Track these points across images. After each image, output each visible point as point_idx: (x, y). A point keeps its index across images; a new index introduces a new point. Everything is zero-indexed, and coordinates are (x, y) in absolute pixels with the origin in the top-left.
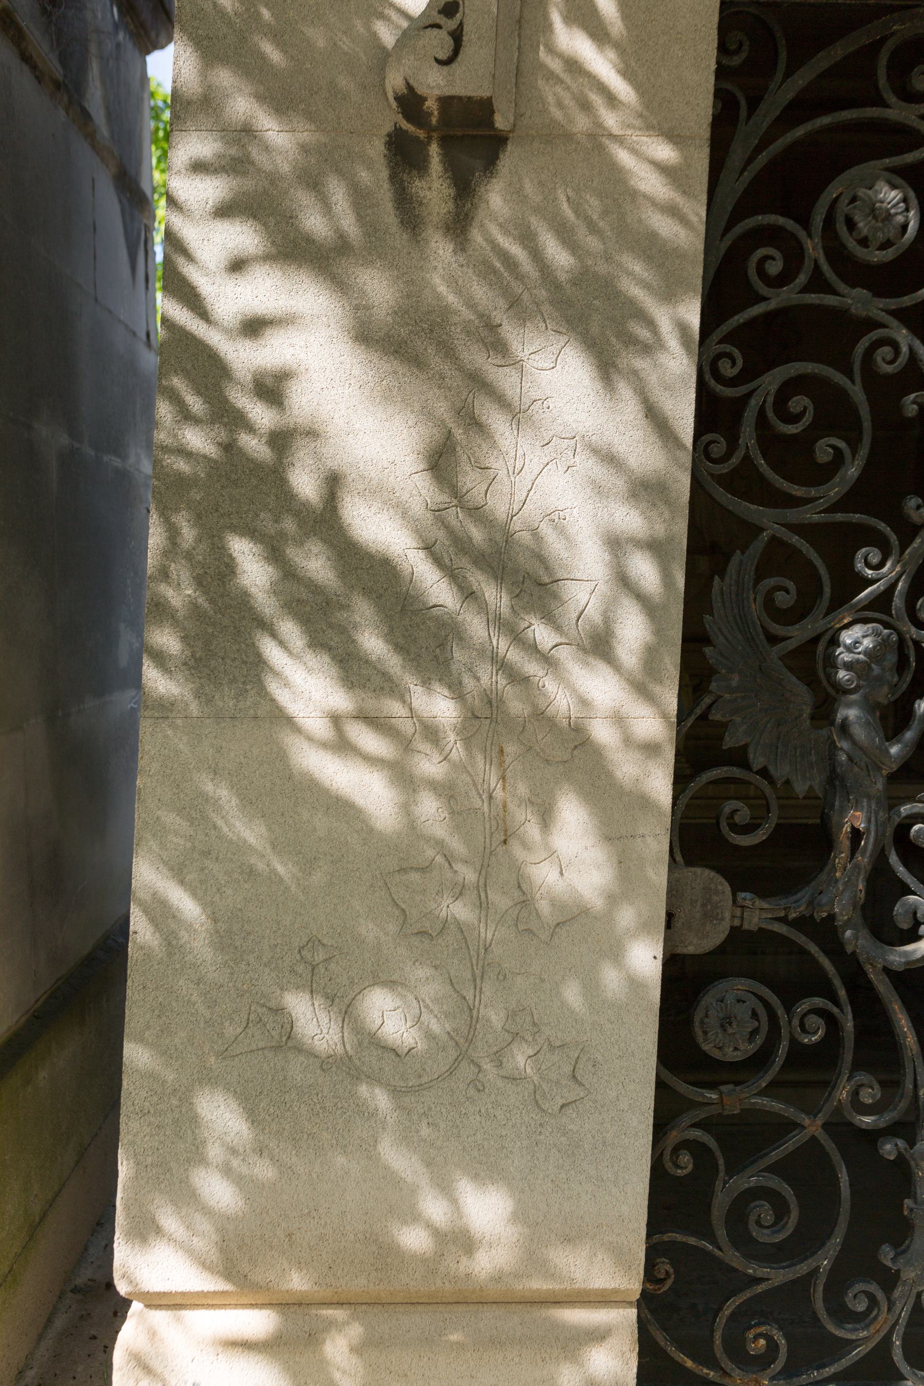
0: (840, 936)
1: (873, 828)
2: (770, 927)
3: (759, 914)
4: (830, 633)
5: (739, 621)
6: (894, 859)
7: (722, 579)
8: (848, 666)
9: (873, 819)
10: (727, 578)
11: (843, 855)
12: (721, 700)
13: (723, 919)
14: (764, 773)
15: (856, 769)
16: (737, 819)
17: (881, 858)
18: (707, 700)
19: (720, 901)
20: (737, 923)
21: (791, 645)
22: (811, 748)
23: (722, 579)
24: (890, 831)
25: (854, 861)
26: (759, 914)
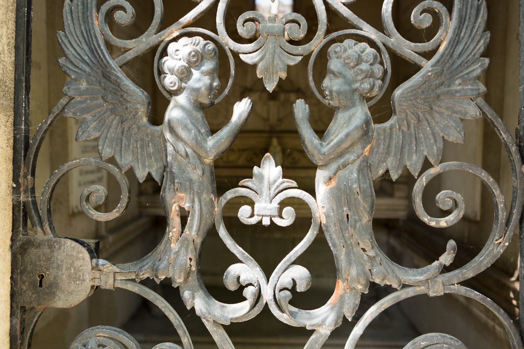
0: (181, 295)
1: (197, 207)
2: (124, 287)
4: (162, 45)
6: (223, 232)
9: (196, 200)
11: (175, 230)
12: (72, 101)
13: (84, 280)
14: (112, 160)
15: (179, 158)
17: (212, 233)
18: (63, 101)
20: (96, 283)
21: (129, 56)
22: (149, 141)
25: (184, 234)
26: (113, 276)
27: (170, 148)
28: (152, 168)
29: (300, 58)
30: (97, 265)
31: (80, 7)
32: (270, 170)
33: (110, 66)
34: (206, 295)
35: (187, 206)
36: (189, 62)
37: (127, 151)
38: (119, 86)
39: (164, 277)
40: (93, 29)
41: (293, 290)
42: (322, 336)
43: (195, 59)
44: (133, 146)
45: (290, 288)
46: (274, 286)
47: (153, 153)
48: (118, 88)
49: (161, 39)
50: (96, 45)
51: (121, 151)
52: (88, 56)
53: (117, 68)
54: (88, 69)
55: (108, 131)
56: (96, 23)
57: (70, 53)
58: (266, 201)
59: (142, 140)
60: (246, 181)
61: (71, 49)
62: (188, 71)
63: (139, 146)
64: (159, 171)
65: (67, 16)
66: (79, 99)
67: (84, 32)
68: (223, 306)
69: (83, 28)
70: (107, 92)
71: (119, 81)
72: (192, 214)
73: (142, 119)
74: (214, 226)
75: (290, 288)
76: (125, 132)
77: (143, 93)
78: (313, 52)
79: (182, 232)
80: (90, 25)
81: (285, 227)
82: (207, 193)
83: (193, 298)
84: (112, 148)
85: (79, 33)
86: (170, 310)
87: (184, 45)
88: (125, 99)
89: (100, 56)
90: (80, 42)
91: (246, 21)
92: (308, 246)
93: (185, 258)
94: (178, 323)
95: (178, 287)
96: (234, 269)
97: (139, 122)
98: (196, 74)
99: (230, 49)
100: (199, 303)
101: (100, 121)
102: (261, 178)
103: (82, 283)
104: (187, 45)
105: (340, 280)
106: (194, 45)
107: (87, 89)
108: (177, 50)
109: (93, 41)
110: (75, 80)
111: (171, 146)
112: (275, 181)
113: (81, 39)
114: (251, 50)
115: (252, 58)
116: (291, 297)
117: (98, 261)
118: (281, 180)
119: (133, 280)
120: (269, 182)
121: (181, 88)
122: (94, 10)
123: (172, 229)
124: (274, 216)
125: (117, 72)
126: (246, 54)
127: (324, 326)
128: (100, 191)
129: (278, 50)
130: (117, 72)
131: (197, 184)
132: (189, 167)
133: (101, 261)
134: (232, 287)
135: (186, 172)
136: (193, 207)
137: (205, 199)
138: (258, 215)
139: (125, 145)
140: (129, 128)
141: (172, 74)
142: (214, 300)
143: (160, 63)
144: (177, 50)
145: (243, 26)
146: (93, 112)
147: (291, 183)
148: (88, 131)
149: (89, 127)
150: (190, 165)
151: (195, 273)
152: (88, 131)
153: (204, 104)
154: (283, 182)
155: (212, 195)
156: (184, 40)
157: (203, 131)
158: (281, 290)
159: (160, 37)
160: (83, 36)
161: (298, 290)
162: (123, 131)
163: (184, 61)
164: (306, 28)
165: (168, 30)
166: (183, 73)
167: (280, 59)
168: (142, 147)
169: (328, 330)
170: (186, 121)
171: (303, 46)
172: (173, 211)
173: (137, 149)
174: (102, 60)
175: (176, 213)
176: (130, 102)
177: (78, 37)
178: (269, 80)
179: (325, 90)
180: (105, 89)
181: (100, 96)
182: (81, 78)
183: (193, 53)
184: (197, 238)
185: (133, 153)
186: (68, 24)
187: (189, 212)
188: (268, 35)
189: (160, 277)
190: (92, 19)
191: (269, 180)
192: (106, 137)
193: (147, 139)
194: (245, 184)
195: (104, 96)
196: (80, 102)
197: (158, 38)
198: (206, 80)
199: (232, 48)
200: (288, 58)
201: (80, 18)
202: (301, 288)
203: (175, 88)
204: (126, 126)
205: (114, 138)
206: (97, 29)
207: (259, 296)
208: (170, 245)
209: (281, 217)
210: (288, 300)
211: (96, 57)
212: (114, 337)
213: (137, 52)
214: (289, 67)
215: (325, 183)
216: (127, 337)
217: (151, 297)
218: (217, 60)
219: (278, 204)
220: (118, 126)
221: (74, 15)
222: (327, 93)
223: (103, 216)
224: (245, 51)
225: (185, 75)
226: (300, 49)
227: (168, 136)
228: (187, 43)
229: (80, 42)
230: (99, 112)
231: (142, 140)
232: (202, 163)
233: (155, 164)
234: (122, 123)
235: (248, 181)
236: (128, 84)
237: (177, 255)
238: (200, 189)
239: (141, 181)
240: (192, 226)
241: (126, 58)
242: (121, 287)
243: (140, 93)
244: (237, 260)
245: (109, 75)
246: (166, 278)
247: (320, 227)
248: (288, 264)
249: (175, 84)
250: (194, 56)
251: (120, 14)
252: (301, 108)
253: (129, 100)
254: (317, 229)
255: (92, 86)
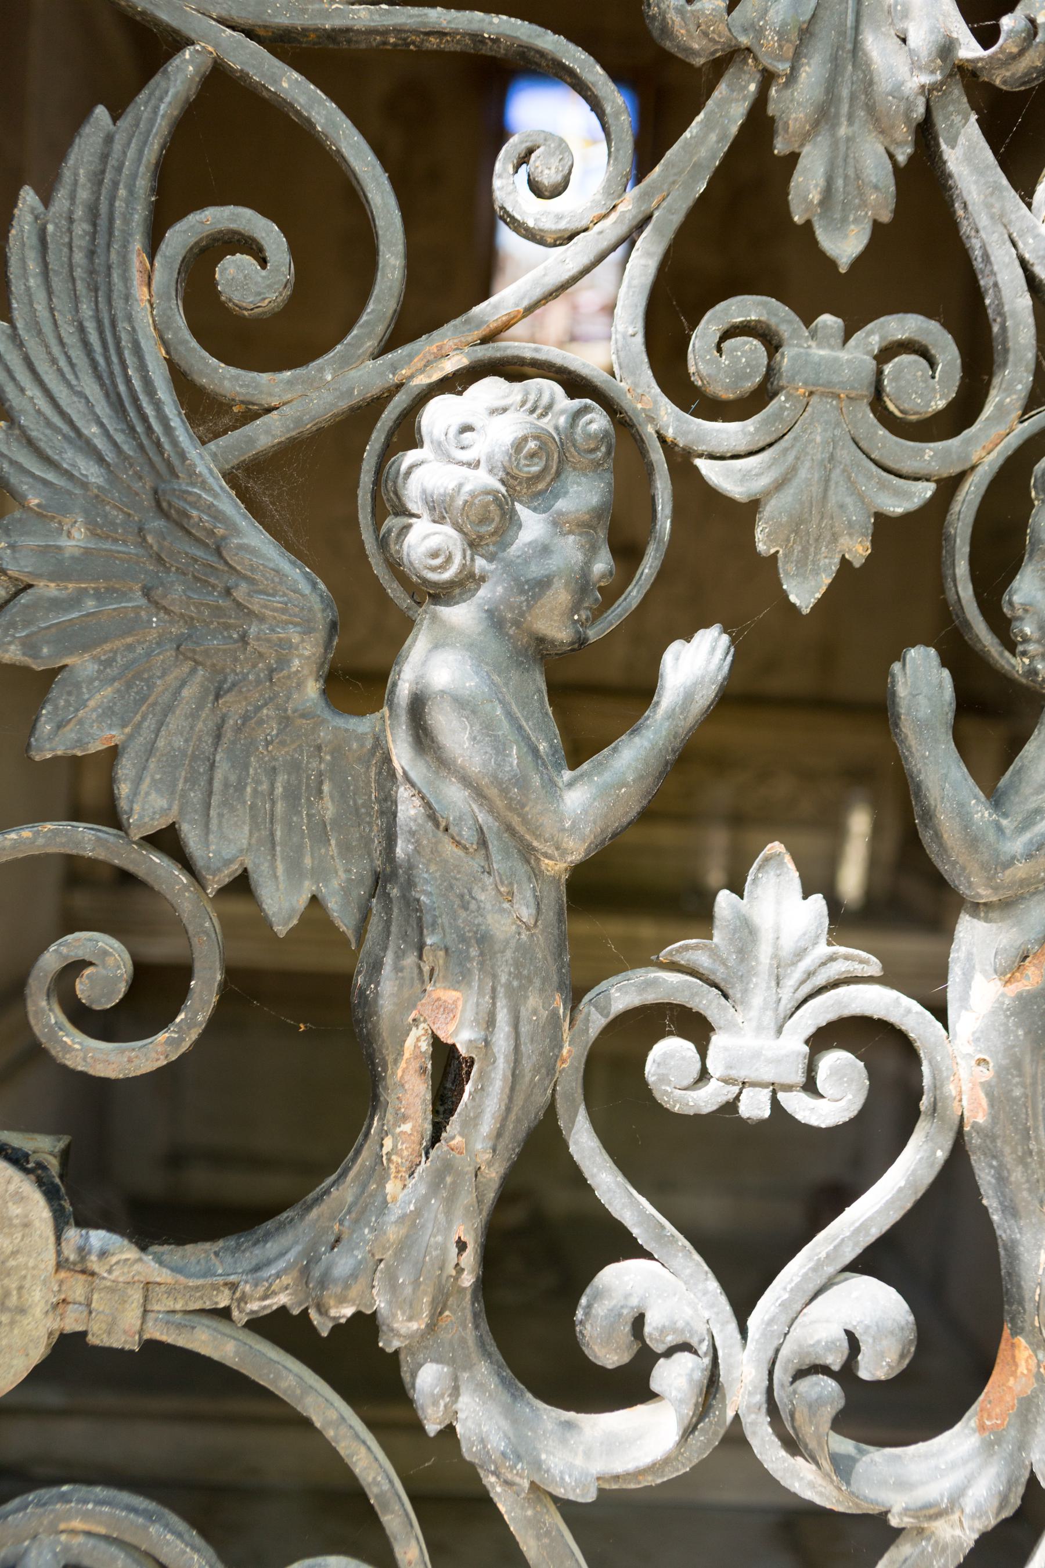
0: (406, 1377)
2: (181, 1340)
3: (136, 1293)
5: (94, 338)
6: (584, 1144)
7: (46, 200)
8: (440, 510)
9: (502, 1016)
10: (61, 196)
11: (406, 1127)
12: (24, 599)
13: (22, 1310)
14: (167, 841)
15: (449, 849)
16: (83, 988)
17: (540, 1147)
19: (14, 1254)
20: (72, 1324)
21: (265, 434)
22: (320, 774)
23: (46, 200)
24: (571, 1054)
25: (441, 1147)
26: (136, 1293)
27: (408, 809)
28: (326, 882)
29: (926, 490)
30: (83, 1252)
31: (81, 228)
32: (776, 909)
33: (191, 473)
34: (503, 1380)
35: (463, 1038)
36: (509, 479)
37: (232, 809)
38: (218, 552)
39: (348, 1311)
40: (130, 318)
41: (847, 1375)
42: (944, 1548)
43: (535, 469)
44: (255, 791)
45: (836, 1367)
46: (770, 1353)
47: (335, 821)
48: (213, 560)
49: (396, 380)
50: (137, 383)
51: (208, 806)
52: (102, 425)
53: (216, 479)
54: (91, 472)
55: (161, 724)
56: (141, 293)
57: (29, 407)
58: (759, 1029)
59: (295, 767)
60: (686, 948)
61: (32, 391)
62: (503, 514)
63: (279, 790)
64: (354, 894)
65: (23, 260)
66: (48, 589)
67: (90, 327)
68: (569, 1425)
69: (86, 310)
70: (168, 570)
71: (220, 531)
72: (481, 1071)
73: (300, 685)
74: (551, 1110)
75: (836, 1367)
76: (228, 734)
77: (314, 585)
78: (973, 468)
79: (435, 1139)
80: (118, 303)
81: (828, 1130)
82: (542, 990)
83: (455, 1392)
84: (173, 793)
85: (68, 331)
86: (357, 1436)
87: (494, 412)
88: (239, 604)
89: (149, 429)
90: (72, 365)
91: (728, 334)
92: (909, 1205)
93: (439, 1239)
94: (386, 1487)
95: (397, 1352)
96: (620, 1282)
97: (288, 698)
98: (532, 526)
99: (662, 439)
100: (466, 1401)
101: (129, 686)
102: (747, 932)
103: (12, 1323)
104: (505, 410)
105: (1021, 1340)
106: (532, 411)
107: (87, 552)
108: (467, 428)
109: (124, 367)
110: (40, 515)
111: (417, 802)
112: (800, 954)
113: (77, 354)
114: (742, 448)
115: (746, 476)
116: (840, 1403)
117: (87, 1238)
118: (823, 949)
119: (225, 1314)
120: (775, 956)
121: (471, 576)
122: (137, 244)
123: (396, 1124)
124: (788, 1088)
125: (216, 496)
126: (722, 458)
127: (955, 1517)
128: (107, 964)
129: (847, 453)
130: (216, 496)
131: (509, 954)
132: (483, 889)
133: (98, 1237)
134: (608, 1353)
135: (473, 906)
136: (487, 1043)
137: (535, 1012)
138: (727, 1081)
139: (226, 785)
140: (246, 718)
141: (440, 520)
142: (529, 1395)
143: (389, 469)
144: (467, 428)
145: (719, 350)
146: (107, 647)
147: (861, 962)
148: (81, 722)
149: (84, 704)
150: (488, 880)
151: (468, 1297)
152: (81, 722)
153: (552, 642)
154: (832, 959)
155: (557, 996)
156: (490, 390)
157: (543, 747)
158: (800, 1374)
159: (394, 368)
160: (86, 344)
161: (864, 1374)
162: (220, 727)
163: (491, 471)
164: (957, 375)
165: (426, 345)
166: (484, 520)
167: (853, 488)
168: (292, 796)
169: (971, 1529)
170: (488, 707)
171: (939, 445)
172: (407, 1055)
173: (273, 803)
174: (158, 445)
175: (415, 1065)
176: (262, 619)
177: (62, 343)
178: (801, 563)
179: (1020, 619)
180: (159, 560)
181: (137, 587)
182: (65, 510)
183: (532, 445)
184: (490, 1164)
185: (253, 818)
186: (28, 289)
187: (471, 1062)
188: (811, 393)
189: (333, 1313)
190: (126, 279)
191: (776, 947)
192: (151, 750)
193: (314, 764)
194: (682, 959)
195: (150, 589)
196: (56, 604)
197: (382, 374)
198: (570, 550)
199: (670, 434)
200: (883, 486)
201: (78, 273)
202: (876, 1365)
203: (447, 575)
204: (234, 706)
205: (184, 753)
206: (144, 319)
207: (712, 1386)
208: (382, 1185)
209: (810, 1086)
210: (828, 1412)
211: (132, 429)
212: (128, 1538)
213: (298, 421)
214: (881, 519)
215: (1000, 972)
216: (179, 1535)
217: (284, 1385)
218: (609, 477)
219: (807, 1042)
220: (200, 707)
221: (51, 257)
222: (1028, 630)
223: (112, 1058)
224: (719, 450)
225: (491, 528)
226: (928, 454)
227: (402, 754)
228: (502, 403)
229: (72, 365)
230: (130, 648)
231: (295, 767)
232: (536, 873)
233: (339, 864)
234: (217, 697)
235: (696, 948)
236: (255, 542)
237: (404, 1224)
238: (518, 976)
239: (281, 930)
240: (478, 1116)
241: (251, 441)
242: (164, 1338)
243: (304, 587)
244: (624, 1245)
245: (181, 504)
246: (358, 1315)
247: (960, 1133)
248: (830, 1270)
249: (449, 559)
250: (532, 455)
251: (239, 268)
252: (921, 682)
253: (256, 608)
254: (948, 1144)
255: (107, 545)
